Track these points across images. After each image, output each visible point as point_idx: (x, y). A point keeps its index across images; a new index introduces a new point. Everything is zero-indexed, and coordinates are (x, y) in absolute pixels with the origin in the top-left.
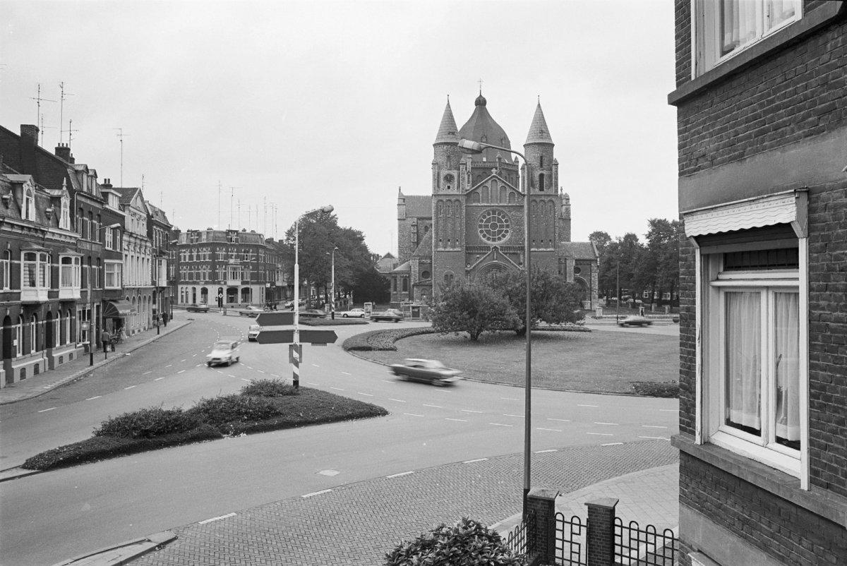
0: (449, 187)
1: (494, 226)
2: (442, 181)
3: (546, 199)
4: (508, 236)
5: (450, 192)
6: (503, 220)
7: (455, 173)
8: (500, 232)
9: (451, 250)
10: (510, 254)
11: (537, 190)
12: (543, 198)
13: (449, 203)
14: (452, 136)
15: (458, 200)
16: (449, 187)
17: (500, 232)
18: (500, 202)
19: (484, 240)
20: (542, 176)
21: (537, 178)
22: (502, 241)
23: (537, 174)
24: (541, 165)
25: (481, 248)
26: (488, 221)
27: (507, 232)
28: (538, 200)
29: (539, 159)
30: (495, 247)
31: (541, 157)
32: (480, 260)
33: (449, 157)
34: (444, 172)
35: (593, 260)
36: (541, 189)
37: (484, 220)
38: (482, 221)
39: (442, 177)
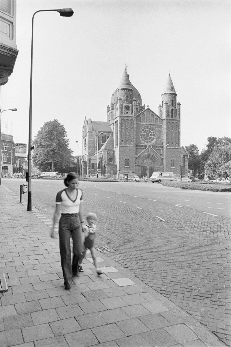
0: (127, 113)
1: (148, 135)
2: (124, 109)
3: (175, 122)
4: (154, 141)
5: (128, 115)
6: (144, 130)
7: (130, 105)
8: (150, 138)
9: (128, 146)
10: (156, 149)
11: (170, 117)
12: (173, 121)
13: (127, 121)
14: (128, 86)
15: (132, 120)
16: (127, 113)
17: (150, 138)
18: (151, 123)
19: (143, 142)
20: (172, 110)
21: (170, 111)
22: (151, 143)
23: (171, 108)
24: (172, 105)
25: (142, 146)
26: (145, 132)
27: (154, 138)
28: (171, 122)
29: (171, 101)
30: (150, 146)
31: (172, 101)
32: (142, 152)
33: (127, 96)
34: (125, 104)
35: (186, 155)
36: (172, 117)
37: (143, 131)
38: (141, 132)
39: (124, 107)
